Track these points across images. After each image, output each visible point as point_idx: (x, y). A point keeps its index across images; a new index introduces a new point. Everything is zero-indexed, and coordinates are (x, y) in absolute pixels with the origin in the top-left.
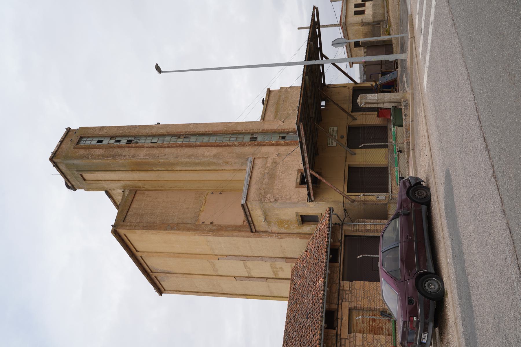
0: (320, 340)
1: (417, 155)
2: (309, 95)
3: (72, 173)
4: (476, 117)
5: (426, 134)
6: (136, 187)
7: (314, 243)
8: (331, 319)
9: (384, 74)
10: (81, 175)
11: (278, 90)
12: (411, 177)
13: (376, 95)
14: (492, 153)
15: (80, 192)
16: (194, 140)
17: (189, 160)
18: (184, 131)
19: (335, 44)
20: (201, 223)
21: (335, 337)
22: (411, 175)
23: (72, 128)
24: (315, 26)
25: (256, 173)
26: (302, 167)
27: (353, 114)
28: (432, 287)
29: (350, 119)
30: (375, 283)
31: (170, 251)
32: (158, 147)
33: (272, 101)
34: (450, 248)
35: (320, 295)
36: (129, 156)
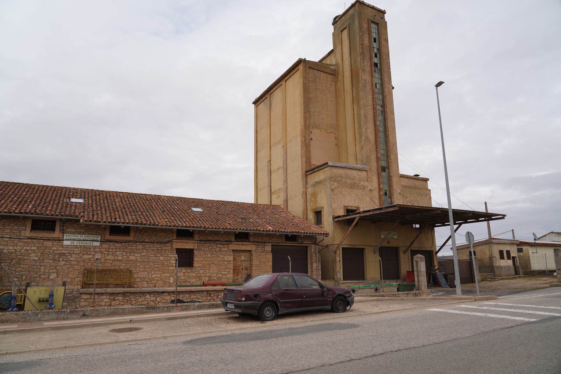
0: (226, 229)
1: (373, 303)
4: (400, 348)
5: (390, 310)
6: (338, 75)
8: (243, 236)
9: (445, 276)
10: (346, 28)
11: (427, 188)
14: (370, 359)
16: (380, 120)
17: (362, 116)
18: (388, 110)
19: (469, 235)
21: (229, 240)
23: (385, 15)
24: (488, 217)
25: (354, 173)
26: (361, 210)
27: (409, 252)
29: (404, 249)
34: (298, 326)
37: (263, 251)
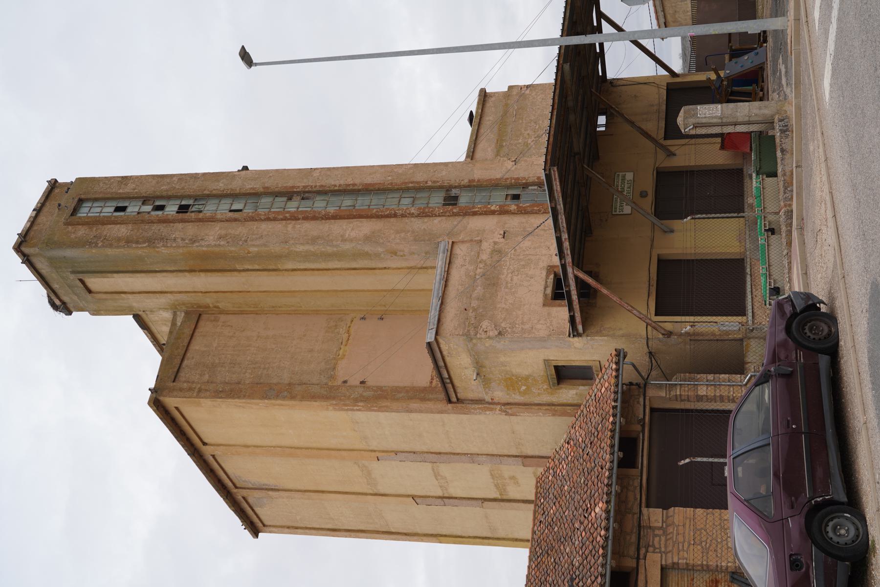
2: (570, 104)
3: (63, 278)
5: (828, 198)
6: (200, 307)
7: (584, 425)
10: (82, 281)
12: (795, 293)
13: (719, 106)
15: (80, 317)
16: (323, 204)
18: (300, 184)
20: (340, 383)
22: (797, 290)
23: (60, 181)
26: (556, 261)
28: (843, 532)
29: (661, 155)
30: (717, 512)
31: (274, 444)
32: (246, 220)
33: (490, 118)
35: (599, 538)
36: (183, 239)
37: (665, 533)
